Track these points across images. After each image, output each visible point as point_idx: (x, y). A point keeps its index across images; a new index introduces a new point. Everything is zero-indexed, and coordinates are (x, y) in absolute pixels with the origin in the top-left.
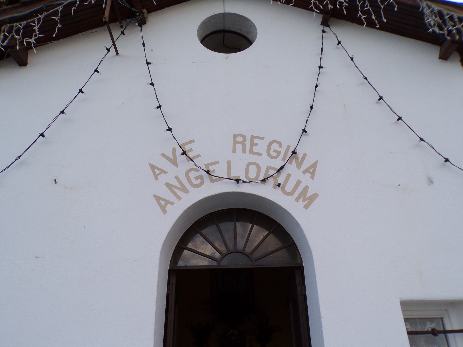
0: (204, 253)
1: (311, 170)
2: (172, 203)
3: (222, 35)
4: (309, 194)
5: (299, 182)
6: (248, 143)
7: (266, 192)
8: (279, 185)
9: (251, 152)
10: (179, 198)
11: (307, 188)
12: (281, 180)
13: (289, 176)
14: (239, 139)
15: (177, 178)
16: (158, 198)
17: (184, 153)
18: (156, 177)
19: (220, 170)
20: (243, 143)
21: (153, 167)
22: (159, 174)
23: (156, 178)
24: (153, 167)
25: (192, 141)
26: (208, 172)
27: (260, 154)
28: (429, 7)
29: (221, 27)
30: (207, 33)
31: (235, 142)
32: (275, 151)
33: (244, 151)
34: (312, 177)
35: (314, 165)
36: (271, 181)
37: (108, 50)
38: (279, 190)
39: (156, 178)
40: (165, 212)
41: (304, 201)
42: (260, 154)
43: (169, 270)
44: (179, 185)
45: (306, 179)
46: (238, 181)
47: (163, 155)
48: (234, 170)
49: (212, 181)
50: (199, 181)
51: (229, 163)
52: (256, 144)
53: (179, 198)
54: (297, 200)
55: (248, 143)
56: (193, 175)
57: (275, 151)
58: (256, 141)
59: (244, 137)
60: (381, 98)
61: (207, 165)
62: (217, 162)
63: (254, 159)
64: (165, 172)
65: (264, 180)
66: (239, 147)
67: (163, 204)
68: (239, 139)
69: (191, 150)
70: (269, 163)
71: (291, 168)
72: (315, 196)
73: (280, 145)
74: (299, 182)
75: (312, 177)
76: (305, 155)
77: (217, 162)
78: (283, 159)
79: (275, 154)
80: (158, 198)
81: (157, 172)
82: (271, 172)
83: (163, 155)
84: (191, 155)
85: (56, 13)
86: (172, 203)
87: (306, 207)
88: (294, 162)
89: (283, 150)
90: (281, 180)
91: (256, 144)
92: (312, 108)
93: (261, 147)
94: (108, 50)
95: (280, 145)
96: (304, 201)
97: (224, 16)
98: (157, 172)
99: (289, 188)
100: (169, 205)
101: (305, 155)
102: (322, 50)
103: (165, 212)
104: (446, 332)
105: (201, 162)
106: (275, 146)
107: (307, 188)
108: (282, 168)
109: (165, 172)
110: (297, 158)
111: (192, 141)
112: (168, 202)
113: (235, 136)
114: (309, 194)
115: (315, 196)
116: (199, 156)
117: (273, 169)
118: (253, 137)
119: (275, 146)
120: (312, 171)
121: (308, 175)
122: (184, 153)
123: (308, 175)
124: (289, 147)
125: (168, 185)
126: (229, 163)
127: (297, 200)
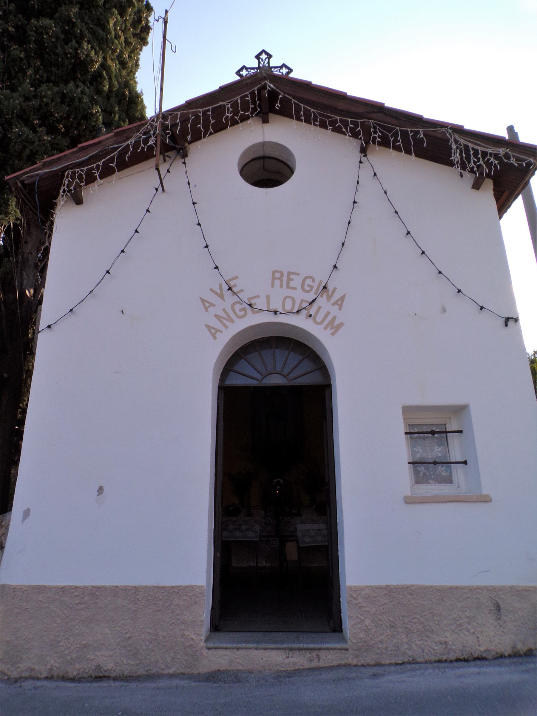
0: (246, 377)
1: (339, 303)
2: (221, 332)
3: (262, 161)
4: (337, 323)
5: (328, 313)
6: (285, 279)
7: (300, 322)
8: (310, 316)
9: (288, 287)
10: (226, 327)
11: (334, 318)
12: (312, 312)
13: (319, 308)
14: (278, 275)
15: (224, 310)
16: (209, 327)
17: (230, 289)
18: (206, 309)
19: (260, 304)
21: (203, 301)
22: (209, 307)
23: (207, 311)
24: (203, 301)
25: (236, 278)
26: (250, 305)
27: (295, 289)
28: (456, 142)
29: (261, 154)
30: (248, 161)
32: (309, 286)
33: (281, 286)
34: (340, 309)
36: (304, 312)
37: (157, 190)
38: (310, 320)
39: (207, 311)
40: (215, 338)
41: (331, 329)
42: (295, 289)
44: (225, 316)
45: (334, 311)
46: (276, 312)
47: (211, 290)
48: (274, 306)
49: (254, 313)
50: (243, 313)
51: (268, 297)
52: (292, 280)
53: (226, 327)
54: (326, 328)
55: (285, 279)
56: (237, 307)
57: (309, 286)
58: (292, 276)
59: (282, 273)
60: (408, 233)
61: (249, 299)
62: (258, 296)
63: (290, 292)
64: (214, 305)
65: (298, 312)
66: (277, 282)
67: (213, 332)
68: (278, 275)
69: (235, 285)
70: (302, 297)
71: (322, 301)
72: (342, 324)
73: (314, 281)
74: (328, 313)
75: (340, 309)
76: (335, 289)
77: (258, 296)
78: (316, 293)
80: (209, 327)
81: (207, 305)
82: (305, 305)
83: (211, 290)
84: (235, 289)
86: (221, 332)
87: (333, 334)
88: (325, 294)
89: (315, 285)
90: (312, 312)
91: (292, 280)
92: (343, 244)
93: (296, 282)
94: (157, 190)
95: (314, 281)
96: (331, 329)
97: (263, 144)
98: (207, 305)
99: (319, 319)
100: (218, 333)
101: (335, 289)
102: (358, 183)
103: (215, 338)
104: (446, 432)
105: (245, 296)
106: (309, 282)
107: (334, 318)
108: (314, 301)
109: (214, 305)
110: (328, 292)
111: (236, 278)
112: (217, 330)
113: (274, 272)
114: (337, 323)
115: (342, 324)
116: (242, 291)
117: (306, 301)
118: (290, 273)
119: (309, 282)
120: (340, 303)
121: (337, 307)
122: (230, 289)
123: (337, 307)
124: (321, 282)
125: (216, 316)
126: (268, 297)
127: (326, 328)
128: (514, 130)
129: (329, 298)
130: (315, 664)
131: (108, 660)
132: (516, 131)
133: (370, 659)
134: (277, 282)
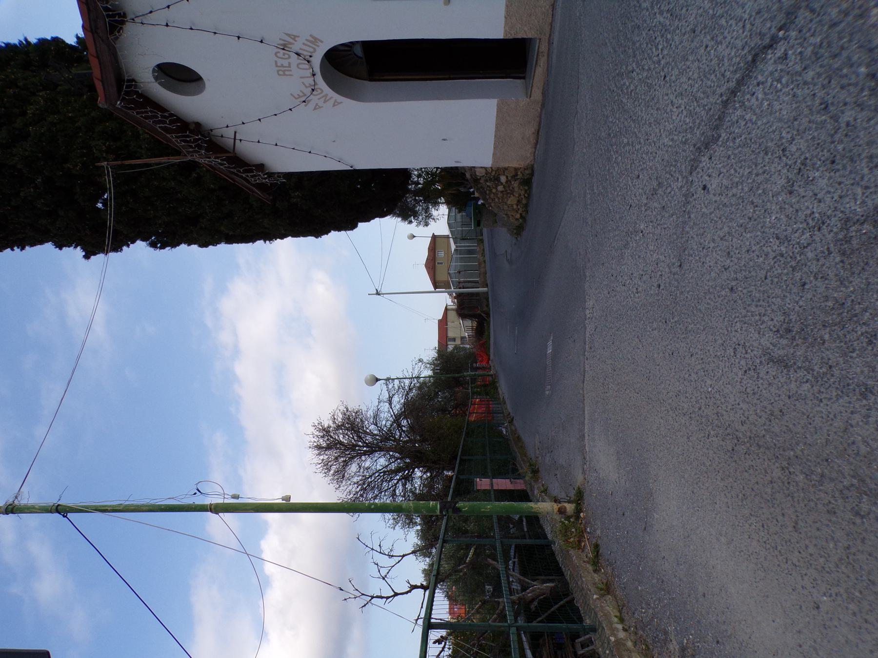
5: (304, 44)
9: (289, 66)
14: (281, 73)
18: (320, 107)
19: (310, 81)
20: (284, 71)
27: (289, 64)
31: (284, 75)
35: (287, 34)
38: (314, 55)
42: (289, 64)
43: (371, 80)
48: (303, 76)
65: (308, 62)
66: (287, 73)
72: (311, 36)
74: (304, 44)
79: (286, 56)
85: (239, 171)
93: (285, 63)
97: (156, 79)
99: (312, 50)
107: (307, 40)
112: (336, 101)
115: (311, 36)
120: (294, 38)
128: (335, 230)
129: (291, 44)
130: (546, 54)
131: (530, 131)
132: (361, 225)
133: (547, 28)
134: (287, 73)
